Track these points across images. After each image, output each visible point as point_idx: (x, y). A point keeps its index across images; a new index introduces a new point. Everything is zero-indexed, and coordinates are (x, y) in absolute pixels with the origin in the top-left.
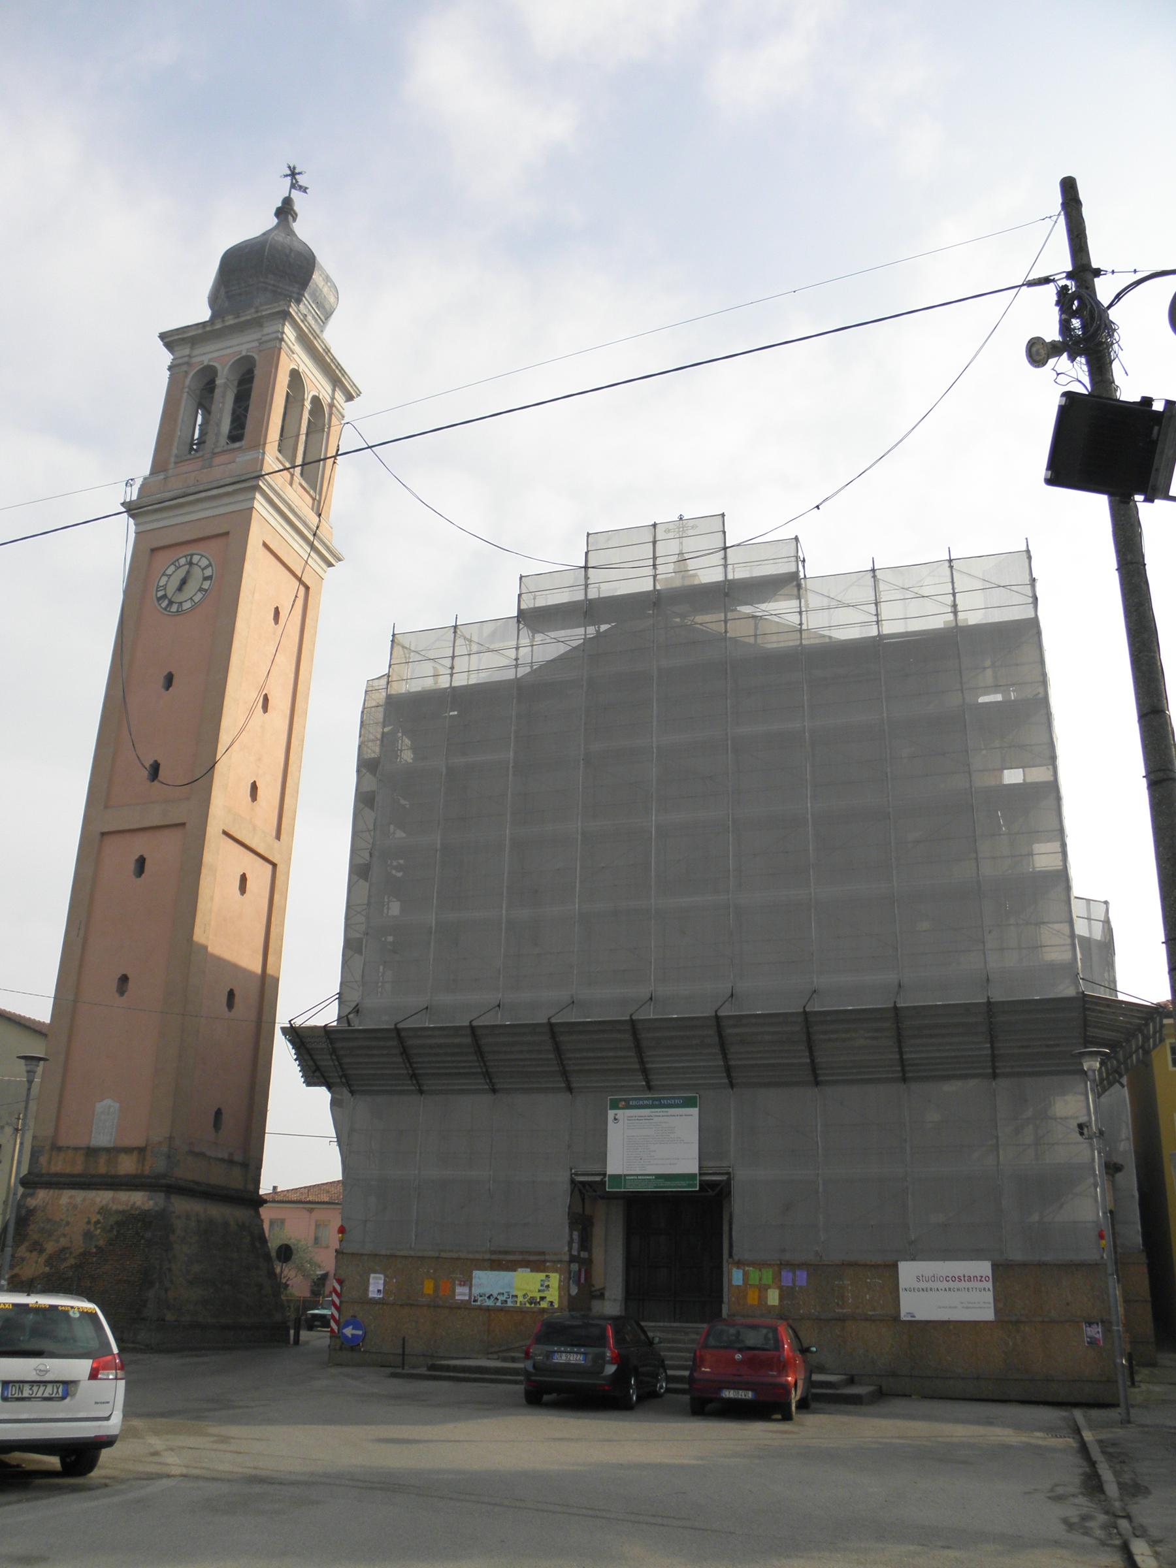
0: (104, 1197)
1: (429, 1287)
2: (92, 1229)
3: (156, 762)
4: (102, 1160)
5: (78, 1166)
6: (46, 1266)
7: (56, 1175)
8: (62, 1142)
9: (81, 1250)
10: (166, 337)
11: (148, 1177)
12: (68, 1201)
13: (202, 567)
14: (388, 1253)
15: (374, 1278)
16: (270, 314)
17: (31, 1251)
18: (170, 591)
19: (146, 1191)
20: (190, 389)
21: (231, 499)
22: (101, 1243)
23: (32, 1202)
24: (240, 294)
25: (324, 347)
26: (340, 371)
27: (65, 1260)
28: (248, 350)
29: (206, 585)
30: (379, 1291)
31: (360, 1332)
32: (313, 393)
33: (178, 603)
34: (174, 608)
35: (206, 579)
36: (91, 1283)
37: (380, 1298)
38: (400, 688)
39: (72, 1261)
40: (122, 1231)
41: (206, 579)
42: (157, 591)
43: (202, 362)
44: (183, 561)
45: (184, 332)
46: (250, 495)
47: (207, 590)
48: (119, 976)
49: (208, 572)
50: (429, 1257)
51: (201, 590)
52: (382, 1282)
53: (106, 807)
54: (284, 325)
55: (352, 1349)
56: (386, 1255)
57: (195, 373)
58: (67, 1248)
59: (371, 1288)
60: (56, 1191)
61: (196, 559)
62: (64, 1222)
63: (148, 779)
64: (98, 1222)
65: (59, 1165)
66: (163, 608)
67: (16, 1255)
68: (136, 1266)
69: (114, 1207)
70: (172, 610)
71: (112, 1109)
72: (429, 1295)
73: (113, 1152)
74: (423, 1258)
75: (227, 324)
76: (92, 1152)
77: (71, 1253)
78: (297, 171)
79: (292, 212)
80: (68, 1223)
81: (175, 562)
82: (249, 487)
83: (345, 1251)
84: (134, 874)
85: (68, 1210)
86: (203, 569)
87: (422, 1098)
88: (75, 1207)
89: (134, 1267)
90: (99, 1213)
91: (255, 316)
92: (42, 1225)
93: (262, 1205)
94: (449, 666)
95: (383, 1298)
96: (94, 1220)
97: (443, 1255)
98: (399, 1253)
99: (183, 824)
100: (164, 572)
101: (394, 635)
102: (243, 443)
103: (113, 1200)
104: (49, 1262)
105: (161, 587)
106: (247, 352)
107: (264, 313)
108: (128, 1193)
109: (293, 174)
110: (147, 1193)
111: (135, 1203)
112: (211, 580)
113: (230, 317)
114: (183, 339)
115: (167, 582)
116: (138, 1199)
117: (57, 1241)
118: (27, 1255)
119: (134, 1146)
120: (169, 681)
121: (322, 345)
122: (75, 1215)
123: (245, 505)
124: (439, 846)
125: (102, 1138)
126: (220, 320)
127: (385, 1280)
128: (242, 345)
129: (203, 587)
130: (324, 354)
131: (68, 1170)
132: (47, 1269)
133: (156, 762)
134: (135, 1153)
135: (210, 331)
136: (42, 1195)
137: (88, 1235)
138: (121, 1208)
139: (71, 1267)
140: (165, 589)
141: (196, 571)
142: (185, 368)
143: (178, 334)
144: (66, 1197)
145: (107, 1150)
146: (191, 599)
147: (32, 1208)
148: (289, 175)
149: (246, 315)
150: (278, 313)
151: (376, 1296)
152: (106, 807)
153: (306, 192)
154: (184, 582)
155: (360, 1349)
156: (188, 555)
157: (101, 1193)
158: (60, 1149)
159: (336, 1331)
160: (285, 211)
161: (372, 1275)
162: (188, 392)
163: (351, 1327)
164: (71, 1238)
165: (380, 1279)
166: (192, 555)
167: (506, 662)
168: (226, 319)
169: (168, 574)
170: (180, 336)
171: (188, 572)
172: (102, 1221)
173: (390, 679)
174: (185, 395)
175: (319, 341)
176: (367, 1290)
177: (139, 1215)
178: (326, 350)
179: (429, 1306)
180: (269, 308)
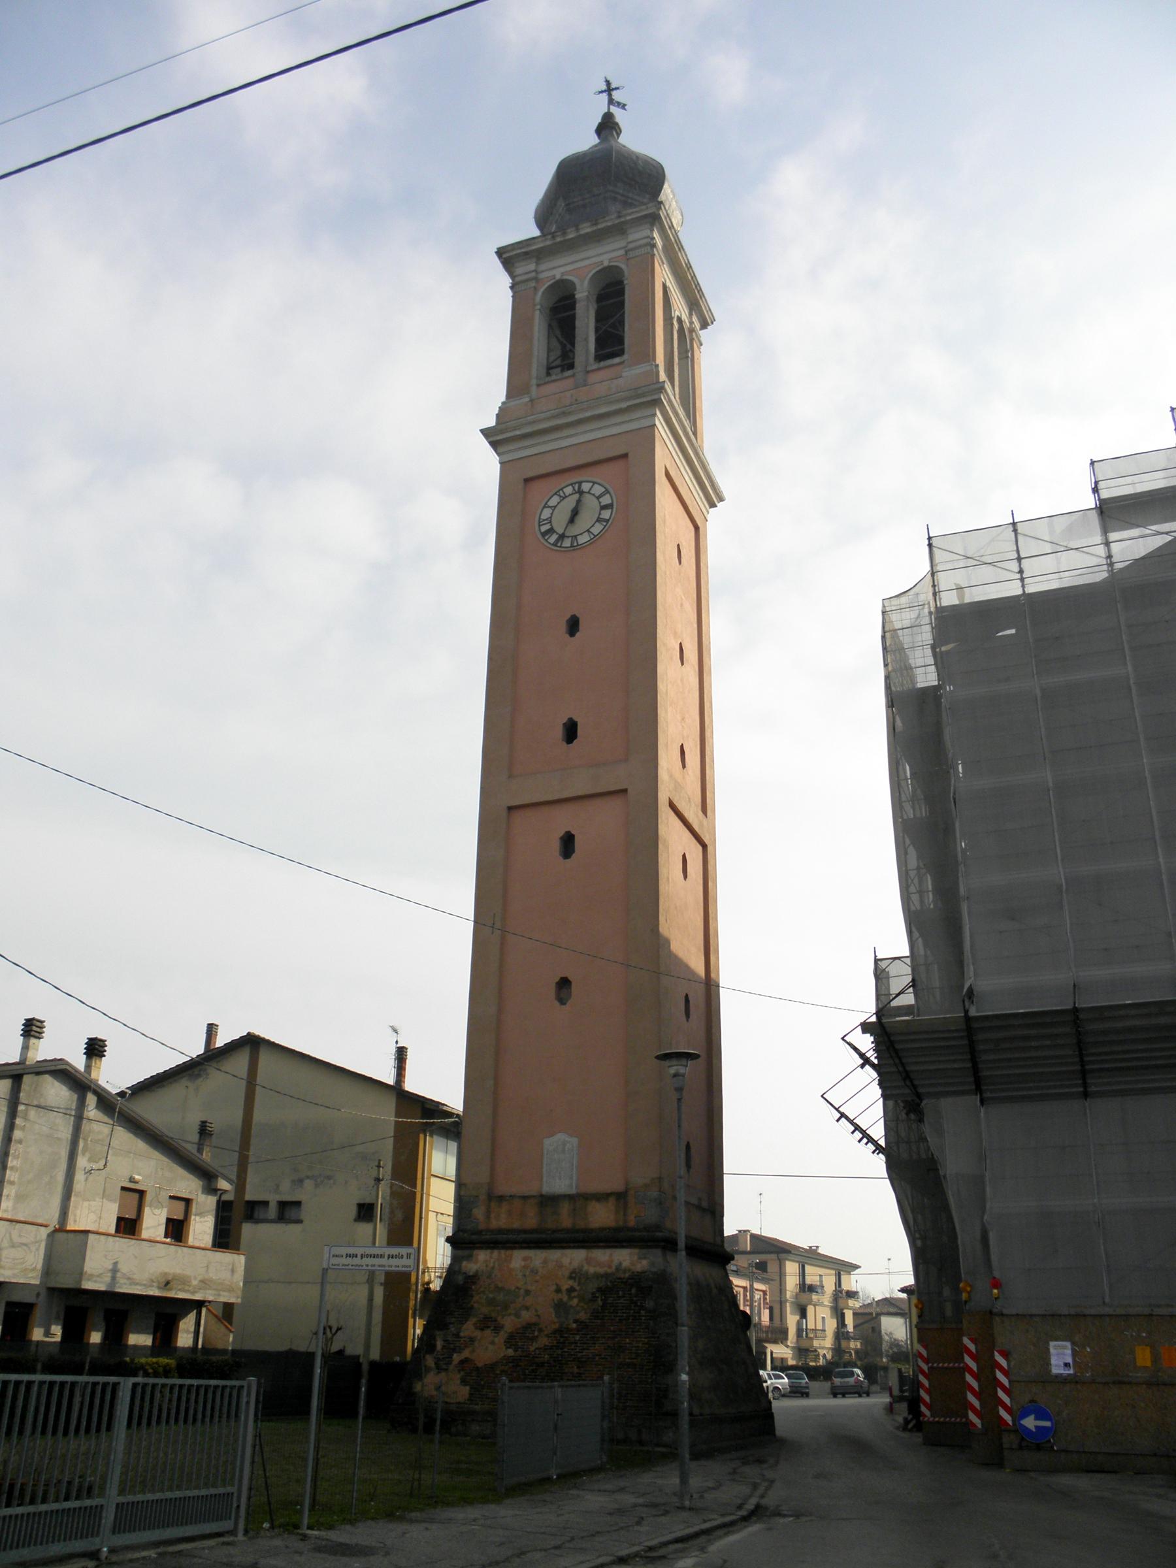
0: (574, 1258)
1: (1143, 1357)
2: (565, 1298)
3: (571, 720)
4: (565, 1208)
5: (531, 1220)
6: (507, 1348)
7: (500, 1231)
8: (503, 1189)
9: (557, 1326)
10: (505, 253)
11: (633, 1229)
12: (523, 1263)
13: (597, 495)
14: (1072, 1312)
15: (1055, 1347)
16: (637, 218)
17: (482, 1330)
18: (559, 525)
19: (635, 1247)
20: (542, 306)
21: (626, 417)
22: (583, 1316)
23: (470, 1267)
24: (584, 206)
25: (687, 262)
26: (698, 292)
27: (534, 1339)
28: (610, 260)
29: (606, 514)
30: (1066, 1365)
31: (1048, 1424)
32: (677, 313)
33: (572, 537)
34: (567, 543)
35: (603, 508)
36: (578, 1367)
37: (1069, 1375)
38: (949, 599)
39: (543, 1341)
40: (610, 1300)
41: (603, 508)
42: (540, 526)
43: (554, 277)
44: (568, 490)
45: (528, 245)
46: (648, 412)
47: (608, 520)
48: (557, 979)
49: (606, 500)
50: (1091, 1315)
51: (599, 520)
52: (1069, 1352)
53: (510, 776)
54: (652, 230)
55: (1038, 1447)
56: (1069, 1315)
57: (546, 289)
58: (535, 1324)
59: (1054, 1361)
60: (503, 1252)
61: (586, 487)
62: (522, 1291)
63: (563, 740)
64: (571, 1290)
65: (502, 1220)
66: (552, 544)
67: (462, 1334)
68: (640, 1345)
69: (592, 1270)
70: (563, 545)
71: (568, 1146)
72: (1146, 1368)
73: (580, 1200)
74: (1127, 1316)
75: (582, 232)
76: (548, 1202)
77: (540, 1330)
78: (613, 86)
79: (617, 128)
80: (528, 1292)
81: (559, 491)
82: (648, 402)
83: (1005, 1311)
84: (560, 855)
85: (525, 1276)
86: (598, 498)
87: (1087, 1104)
88: (534, 1272)
89: (638, 1347)
90: (571, 1278)
91: (617, 222)
92: (491, 1296)
93: (730, 1262)
94: (1017, 570)
95: (1075, 1375)
96: (565, 1287)
97: (1157, 1311)
98: (1087, 1312)
99: (625, 791)
100: (546, 503)
101: (930, 538)
102: (625, 357)
103: (588, 1260)
104: (511, 1341)
105: (544, 520)
106: (610, 262)
107: (628, 218)
108: (608, 1251)
109: (609, 89)
110: (636, 1251)
111: (620, 1264)
112: (612, 509)
113: (585, 225)
114: (526, 253)
115: (552, 514)
116: (625, 1259)
117: (517, 1315)
118: (478, 1334)
119: (609, 1191)
120: (573, 626)
121: (685, 259)
122: (537, 1281)
123: (646, 423)
124: (1051, 784)
125: (559, 1183)
126: (573, 229)
127: (1073, 1350)
128: (605, 254)
129: (601, 517)
130: (686, 269)
131: (516, 1225)
132: (510, 1352)
133: (571, 720)
134: (612, 1200)
135: (560, 242)
136: (482, 1260)
137: (560, 1307)
138: (601, 1271)
139: (545, 1348)
140: (550, 522)
141: (590, 504)
142: (533, 284)
143: (521, 248)
144: (518, 1259)
145: (570, 1197)
146: (588, 531)
147: (471, 1274)
148: (613, 89)
149: (606, 221)
150: (645, 217)
151: (1062, 1372)
152: (510, 776)
153: (625, 109)
154: (575, 513)
155: (1052, 1447)
156: (575, 483)
157: (568, 1252)
158: (501, 1198)
159: (1011, 1423)
160: (607, 126)
161: (1052, 1344)
162: (540, 310)
163: (1032, 1417)
164: (536, 1311)
165: (1065, 1347)
166: (580, 483)
167: (1095, 561)
168: (581, 226)
169: (551, 505)
170: (523, 250)
171: (579, 501)
172: (578, 1288)
173: (937, 588)
174: (537, 313)
175: (683, 254)
176: (1047, 1363)
177: (629, 1279)
178: (689, 266)
179: (1149, 1384)
180: (636, 212)
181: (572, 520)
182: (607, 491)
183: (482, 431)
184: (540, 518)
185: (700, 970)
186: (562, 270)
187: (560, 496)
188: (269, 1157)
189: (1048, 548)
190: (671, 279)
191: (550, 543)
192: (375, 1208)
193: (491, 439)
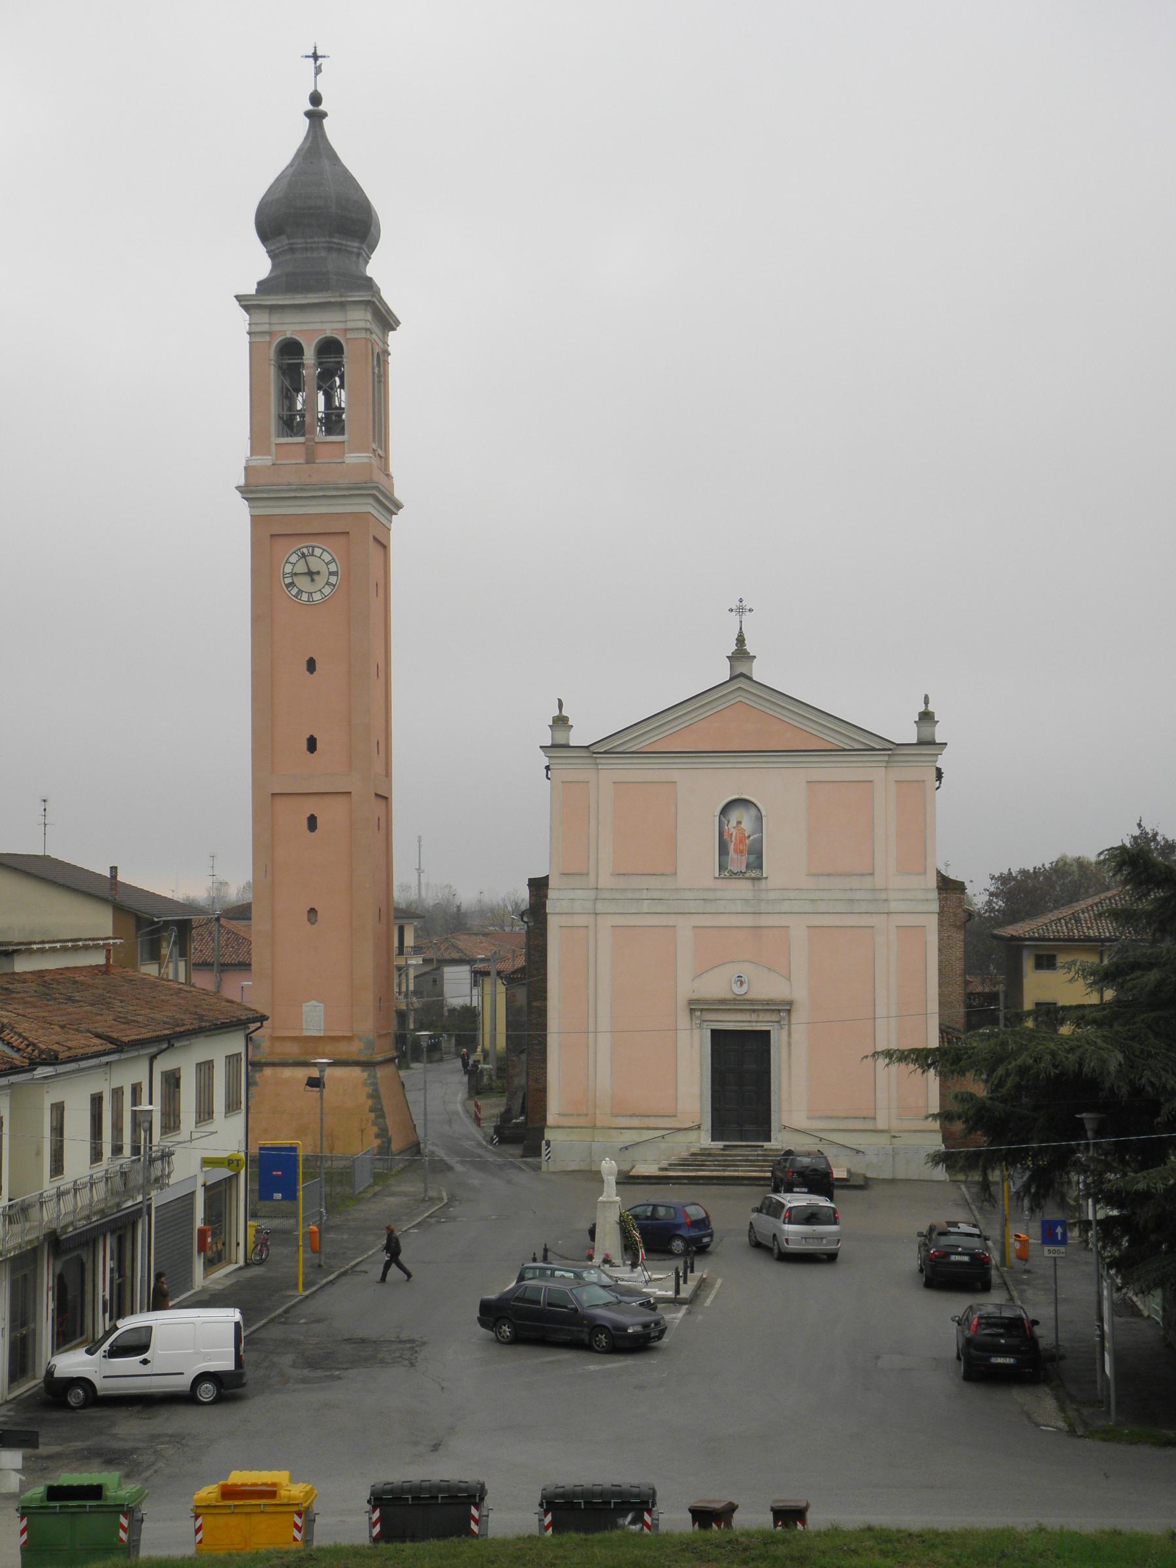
86: (327, 564)
112: (337, 576)
166: (313, 547)
182: (334, 560)
183: (237, 297)
186: (298, 327)
188: (401, 1165)
189: (97, 1045)
193: (243, 303)
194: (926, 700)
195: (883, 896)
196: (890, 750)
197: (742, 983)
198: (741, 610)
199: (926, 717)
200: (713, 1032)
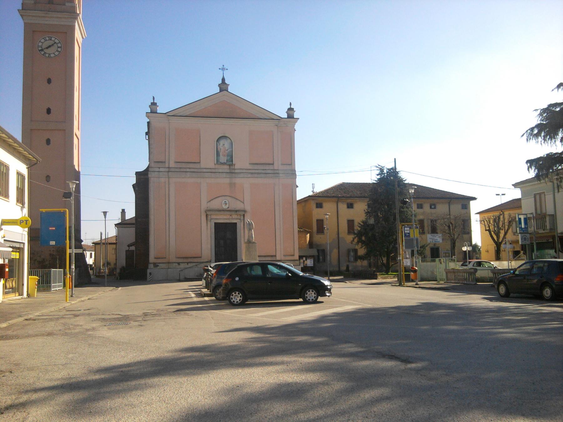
21: (519, 312)
29: (59, 49)
34: (43, 53)
181: (47, 48)
182: (60, 42)
184: (38, 45)
185: (78, 170)
187: (49, 39)
190: (509, 335)
191: (41, 54)
192: (256, 300)
194: (291, 104)
195: (277, 172)
196: (279, 120)
197: (226, 204)
198: (223, 69)
199: (291, 110)
200: (215, 223)
